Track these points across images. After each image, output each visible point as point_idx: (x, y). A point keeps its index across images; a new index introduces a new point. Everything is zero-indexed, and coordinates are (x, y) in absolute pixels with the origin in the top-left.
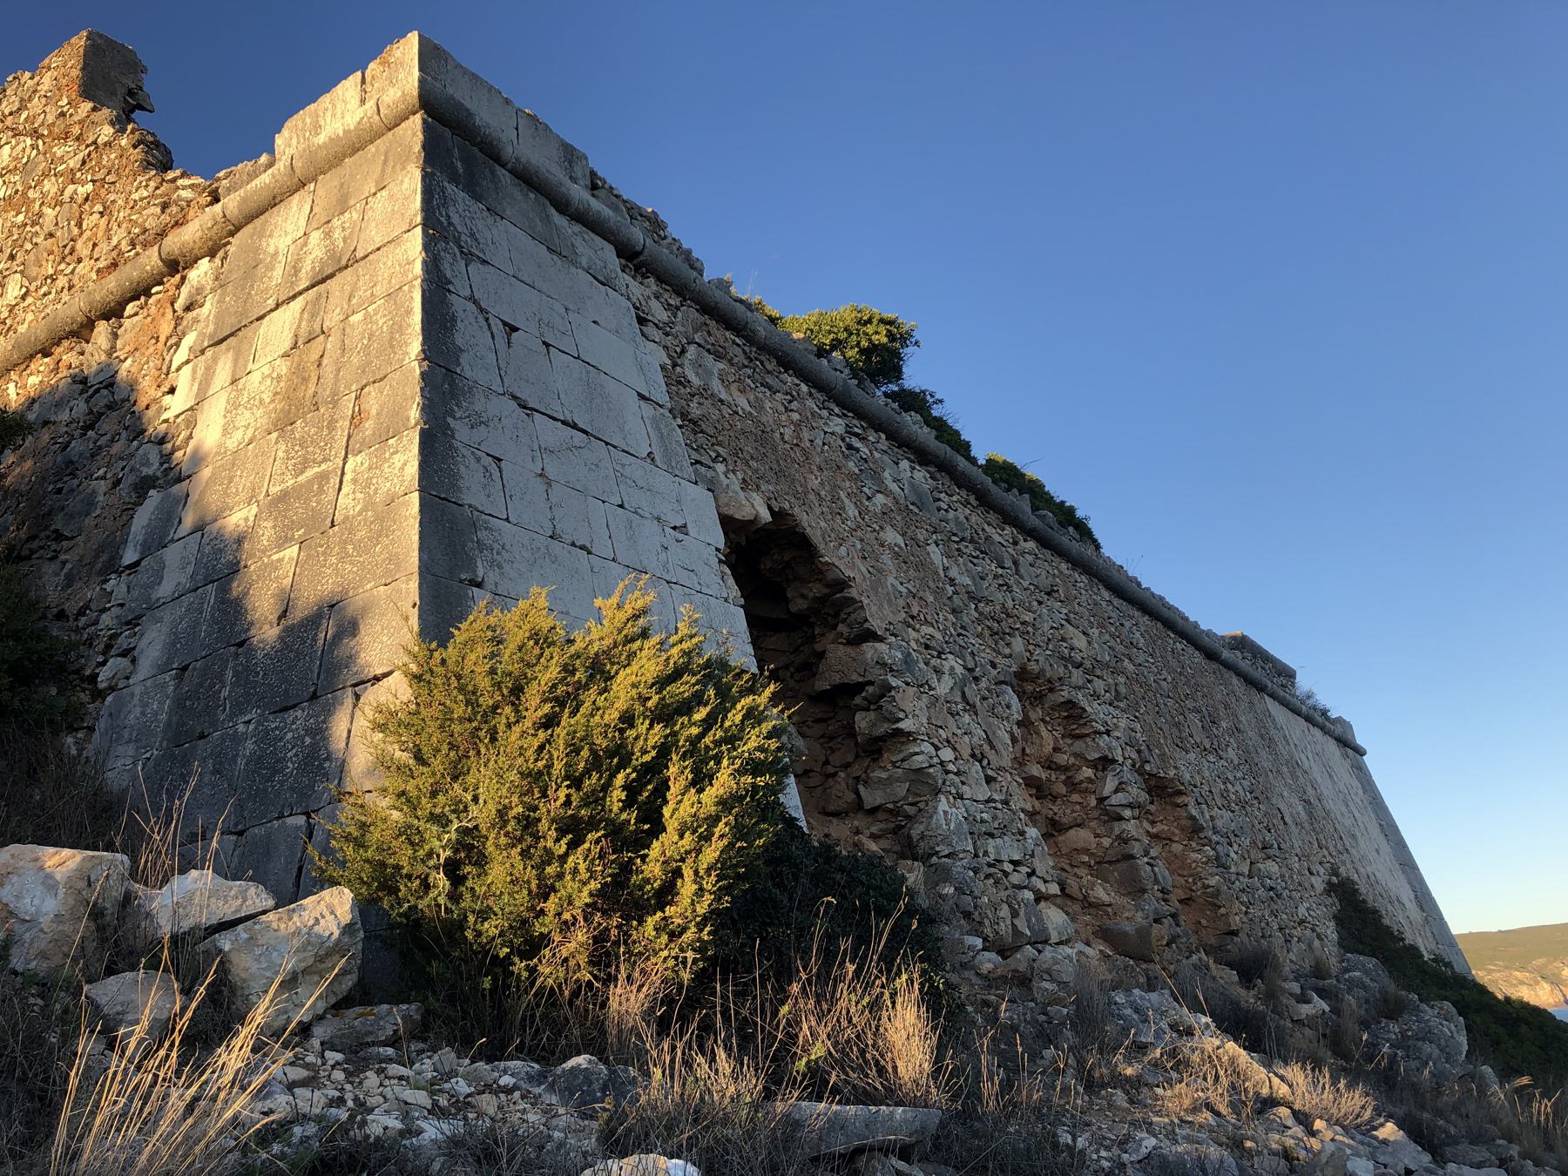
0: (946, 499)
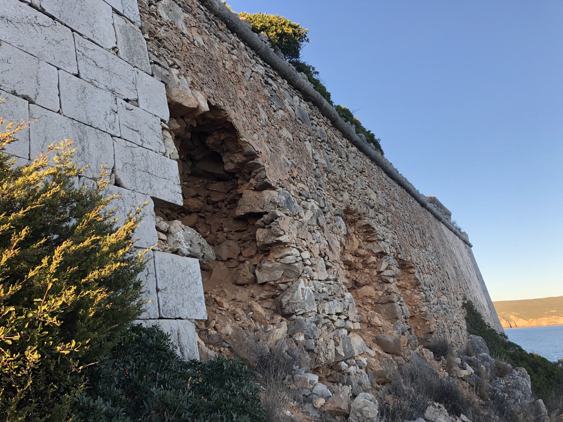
0: (317, 119)
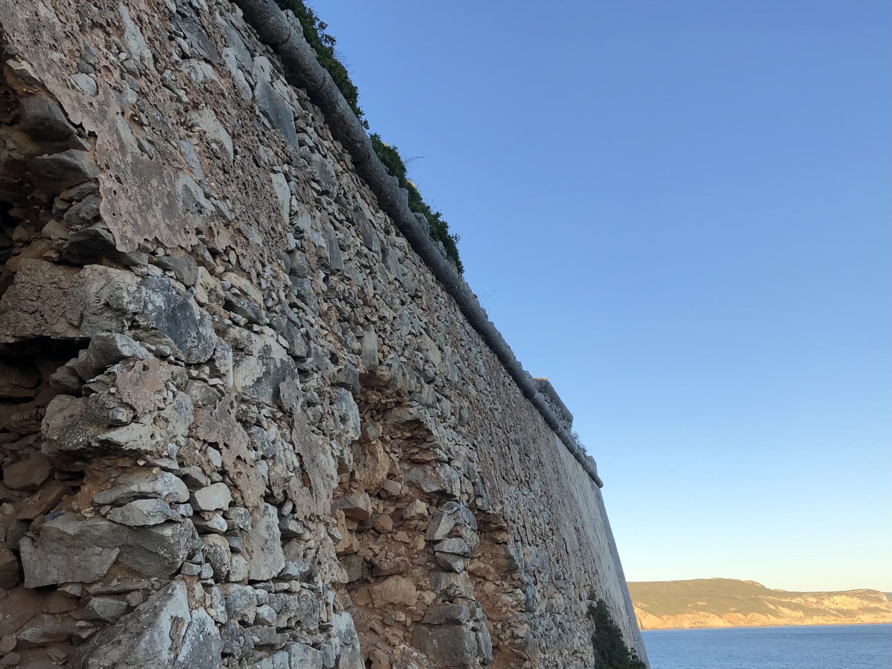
0: (315, 136)
